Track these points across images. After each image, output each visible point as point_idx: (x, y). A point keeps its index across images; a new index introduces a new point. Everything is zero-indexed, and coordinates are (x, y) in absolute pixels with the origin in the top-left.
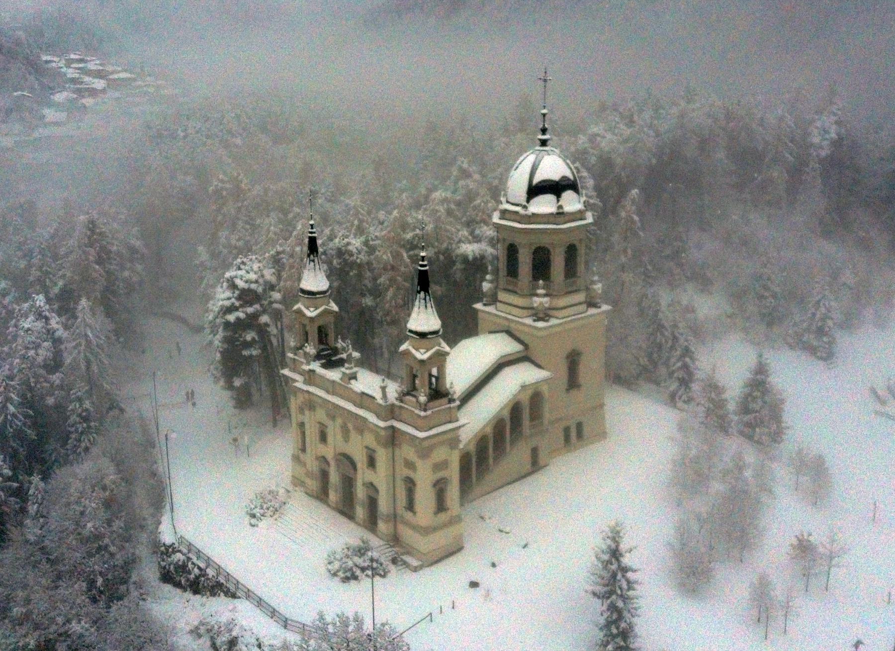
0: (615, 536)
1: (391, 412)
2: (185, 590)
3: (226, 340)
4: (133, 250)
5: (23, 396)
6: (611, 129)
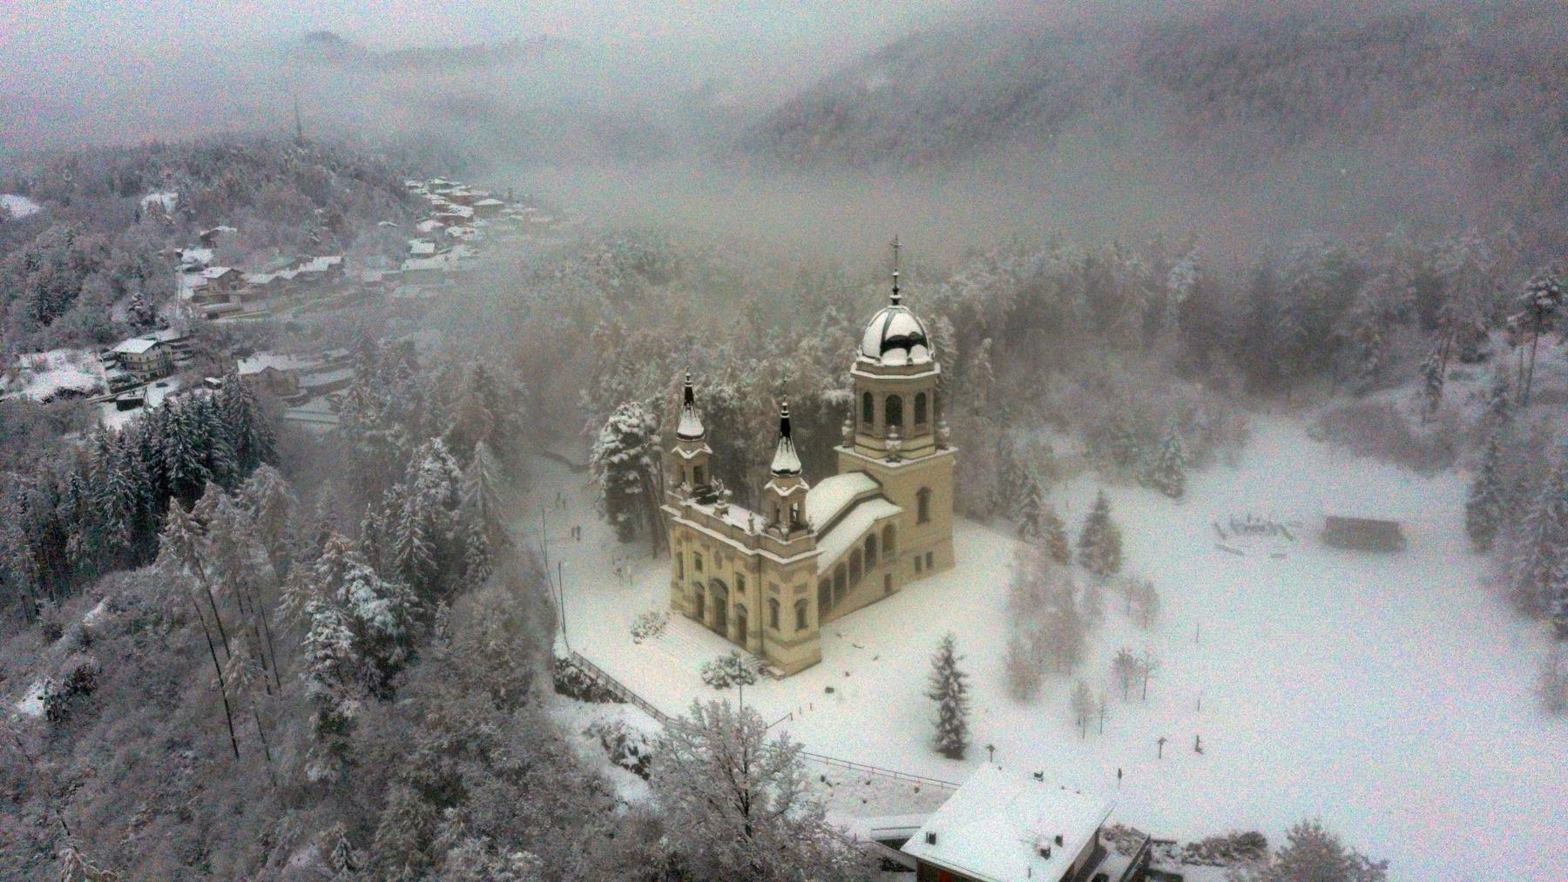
0: (948, 645)
1: (756, 542)
3: (610, 479)
4: (517, 393)
5: (426, 530)
6: (973, 276)
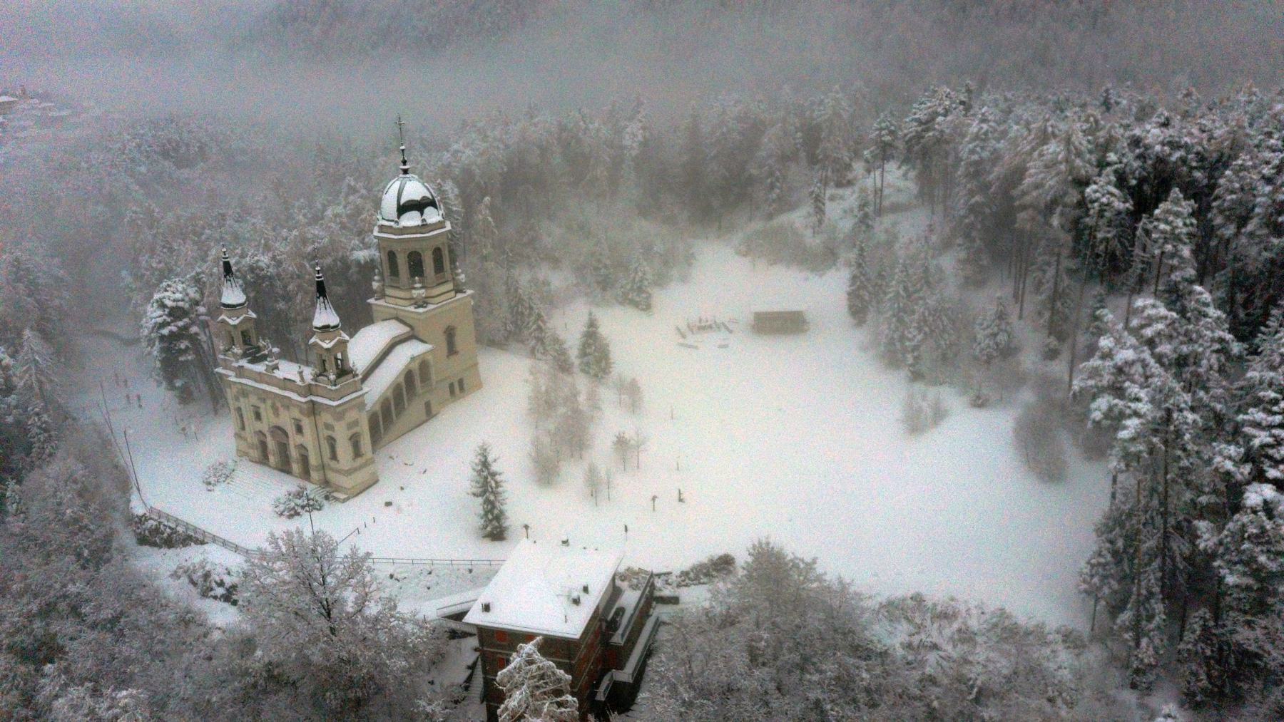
0: (484, 453)
1: (309, 390)
2: (160, 547)
3: (162, 350)
4: (59, 280)
